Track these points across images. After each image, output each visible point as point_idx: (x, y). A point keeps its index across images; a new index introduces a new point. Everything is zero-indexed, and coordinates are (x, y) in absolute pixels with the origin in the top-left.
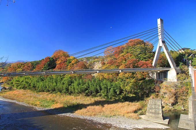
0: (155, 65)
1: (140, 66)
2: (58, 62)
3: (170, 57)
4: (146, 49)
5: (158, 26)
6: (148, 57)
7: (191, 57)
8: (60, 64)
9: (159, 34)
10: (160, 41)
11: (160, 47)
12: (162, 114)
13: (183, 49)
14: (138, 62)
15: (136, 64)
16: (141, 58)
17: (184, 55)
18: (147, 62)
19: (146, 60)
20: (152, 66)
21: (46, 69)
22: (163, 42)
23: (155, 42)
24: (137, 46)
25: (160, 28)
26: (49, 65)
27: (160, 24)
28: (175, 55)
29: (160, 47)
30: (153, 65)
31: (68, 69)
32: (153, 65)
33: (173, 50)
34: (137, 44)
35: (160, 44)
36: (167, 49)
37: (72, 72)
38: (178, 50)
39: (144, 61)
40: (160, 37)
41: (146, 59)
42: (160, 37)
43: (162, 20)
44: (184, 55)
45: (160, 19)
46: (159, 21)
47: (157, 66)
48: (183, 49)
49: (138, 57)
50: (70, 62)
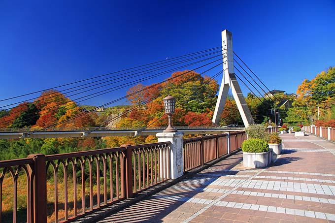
0: (218, 122)
1: (187, 122)
2: (43, 113)
3: (242, 106)
4: (203, 90)
5: (223, 45)
6: (206, 105)
7: (284, 106)
8: (44, 118)
9: (225, 59)
10: (226, 74)
11: (227, 86)
12: (3, 186)
13: (273, 93)
14: (184, 115)
15: (180, 117)
16: (193, 107)
17: (273, 102)
18: (203, 115)
19: (203, 110)
20: (211, 123)
21: (18, 126)
22: (232, 76)
23: (132, 83)
24: (187, 83)
25: (226, 48)
26: (25, 118)
27: (226, 42)
28: (254, 103)
29: (227, 86)
30: (214, 121)
31: (58, 128)
32: (214, 121)
33: (252, 93)
34: (188, 81)
35: (226, 79)
36: (238, 90)
37: (82, 132)
38: (262, 94)
39: (198, 114)
40: (226, 66)
41: (203, 108)
42: (226, 66)
43: (228, 34)
44: (273, 102)
45: (225, 30)
46: (224, 34)
47: (220, 123)
48: (273, 93)
49: (188, 105)
50: (64, 114)
